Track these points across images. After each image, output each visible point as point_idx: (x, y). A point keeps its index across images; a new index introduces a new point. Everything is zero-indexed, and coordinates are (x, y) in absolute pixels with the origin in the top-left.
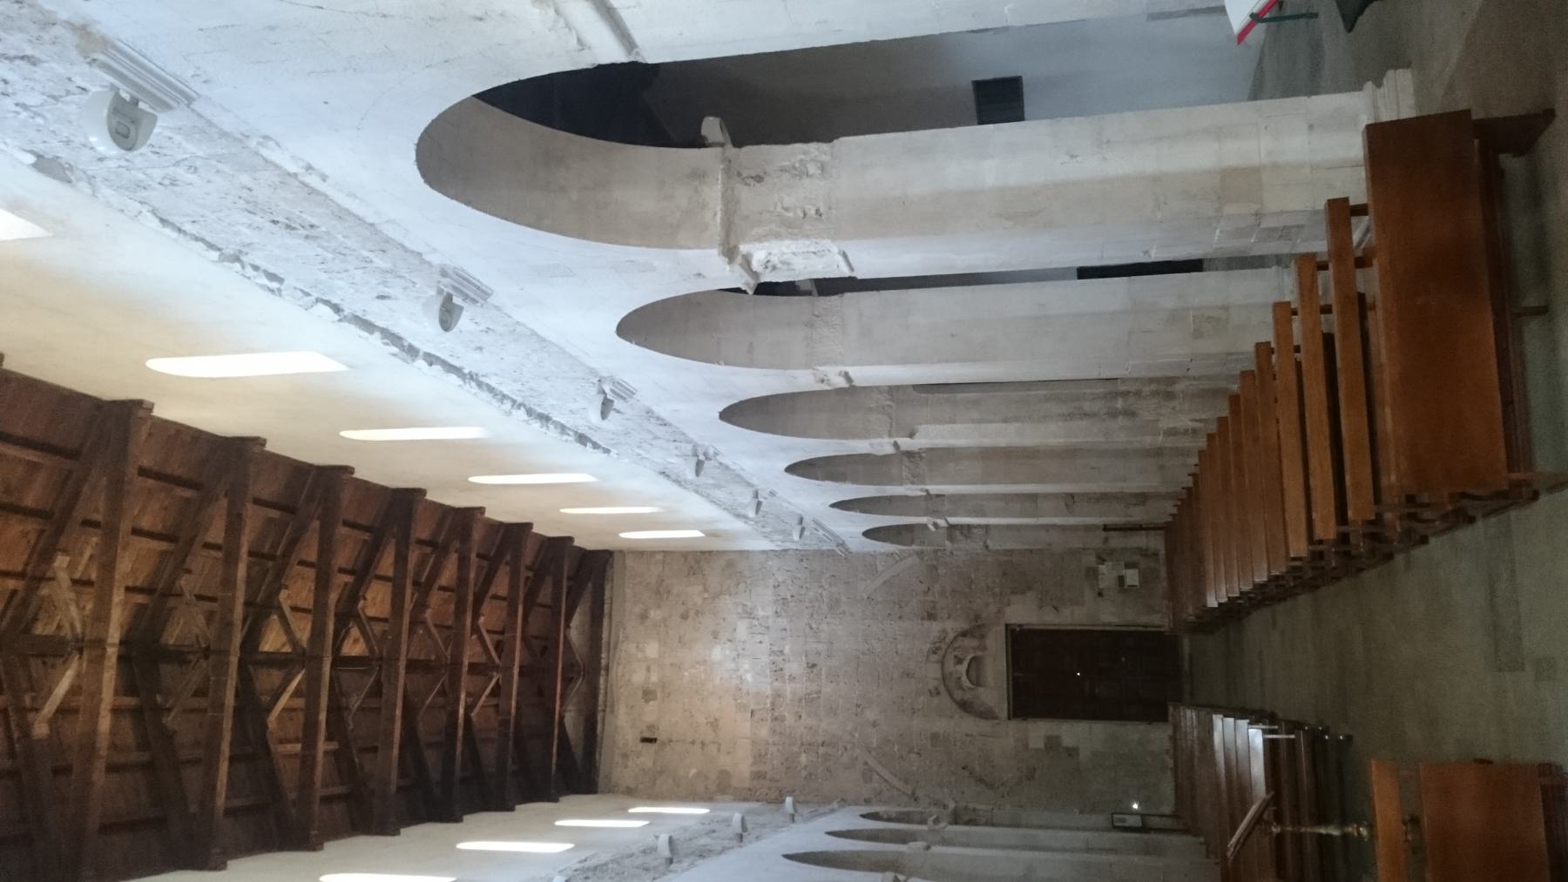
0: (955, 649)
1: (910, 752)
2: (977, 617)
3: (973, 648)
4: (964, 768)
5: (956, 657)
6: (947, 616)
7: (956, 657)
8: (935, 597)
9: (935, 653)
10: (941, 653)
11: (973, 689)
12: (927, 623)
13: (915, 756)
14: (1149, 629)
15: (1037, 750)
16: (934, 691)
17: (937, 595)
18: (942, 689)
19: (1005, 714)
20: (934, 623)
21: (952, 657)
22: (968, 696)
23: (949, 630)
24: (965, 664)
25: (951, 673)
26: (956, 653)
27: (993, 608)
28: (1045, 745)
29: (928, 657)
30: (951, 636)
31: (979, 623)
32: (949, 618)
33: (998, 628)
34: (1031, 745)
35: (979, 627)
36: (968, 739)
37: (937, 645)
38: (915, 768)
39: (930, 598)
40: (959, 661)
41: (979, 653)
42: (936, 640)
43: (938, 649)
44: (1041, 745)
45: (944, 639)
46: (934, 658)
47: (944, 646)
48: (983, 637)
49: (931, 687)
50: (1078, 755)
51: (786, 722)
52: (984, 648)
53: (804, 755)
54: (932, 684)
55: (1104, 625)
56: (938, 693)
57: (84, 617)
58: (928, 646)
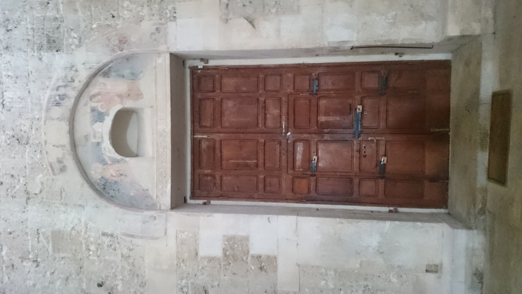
0: (92, 98)
1: (23, 259)
2: (123, 41)
3: (120, 96)
4: (100, 285)
5: (93, 110)
6: (76, 42)
7: (93, 110)
8: (58, 10)
9: (58, 104)
10: (69, 103)
11: (118, 161)
12: (46, 56)
13: (30, 264)
14: (407, 58)
15: (211, 259)
16: (57, 166)
17: (61, 7)
18: (70, 163)
19: (166, 200)
20: (57, 56)
21: (89, 110)
22: (111, 172)
23: (80, 67)
24: (109, 121)
25: (86, 137)
26: (94, 105)
27: (147, 26)
28: (225, 250)
29: (48, 110)
30: (83, 75)
31: (125, 52)
32: (79, 46)
33: (160, 61)
34: (202, 253)
35: (128, 58)
36: (107, 240)
37: (62, 91)
38: (30, 283)
39: (51, 14)
40: (100, 117)
41: (129, 104)
42: (61, 84)
43: (63, 97)
44: (218, 253)
45: (73, 81)
46: (57, 112)
47: (73, 94)
48: (134, 76)
49: (53, 159)
50: (275, 269)
51: (356, 90)
52: (139, 95)
53: (284, 134)
54: (55, 154)
55: (335, 51)
56: (63, 169)
57: (166, 43)
58: (48, 93)
